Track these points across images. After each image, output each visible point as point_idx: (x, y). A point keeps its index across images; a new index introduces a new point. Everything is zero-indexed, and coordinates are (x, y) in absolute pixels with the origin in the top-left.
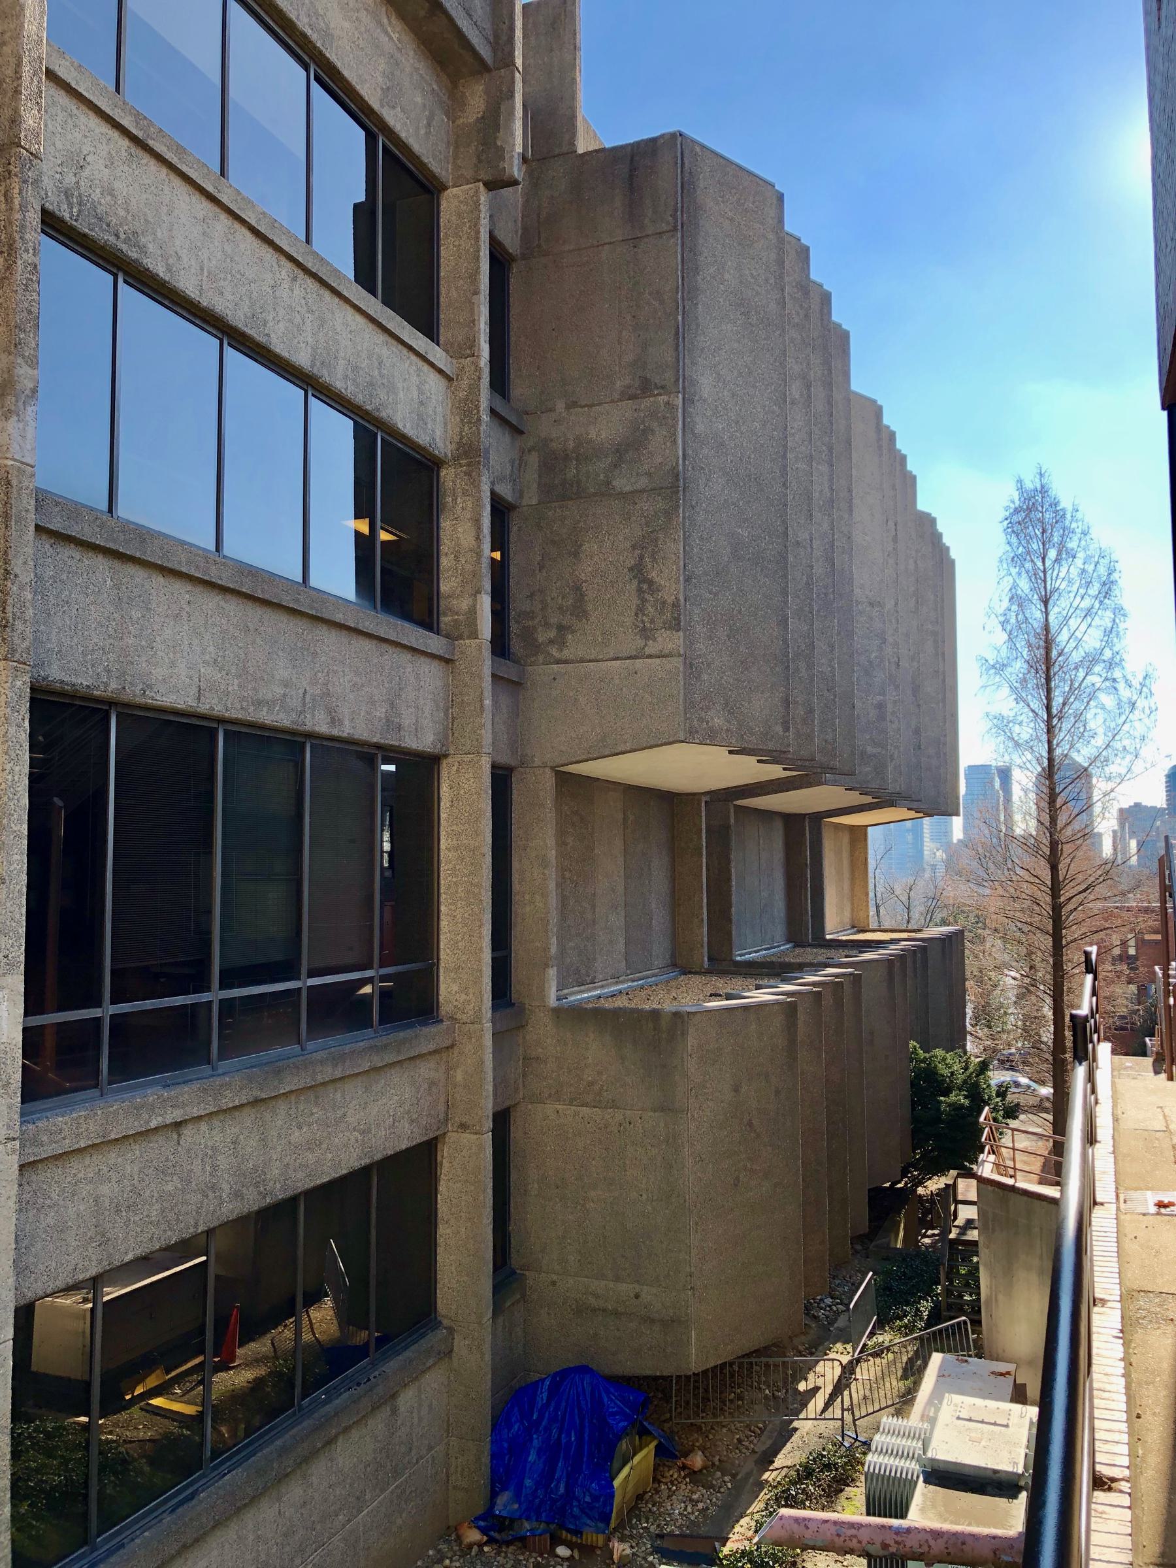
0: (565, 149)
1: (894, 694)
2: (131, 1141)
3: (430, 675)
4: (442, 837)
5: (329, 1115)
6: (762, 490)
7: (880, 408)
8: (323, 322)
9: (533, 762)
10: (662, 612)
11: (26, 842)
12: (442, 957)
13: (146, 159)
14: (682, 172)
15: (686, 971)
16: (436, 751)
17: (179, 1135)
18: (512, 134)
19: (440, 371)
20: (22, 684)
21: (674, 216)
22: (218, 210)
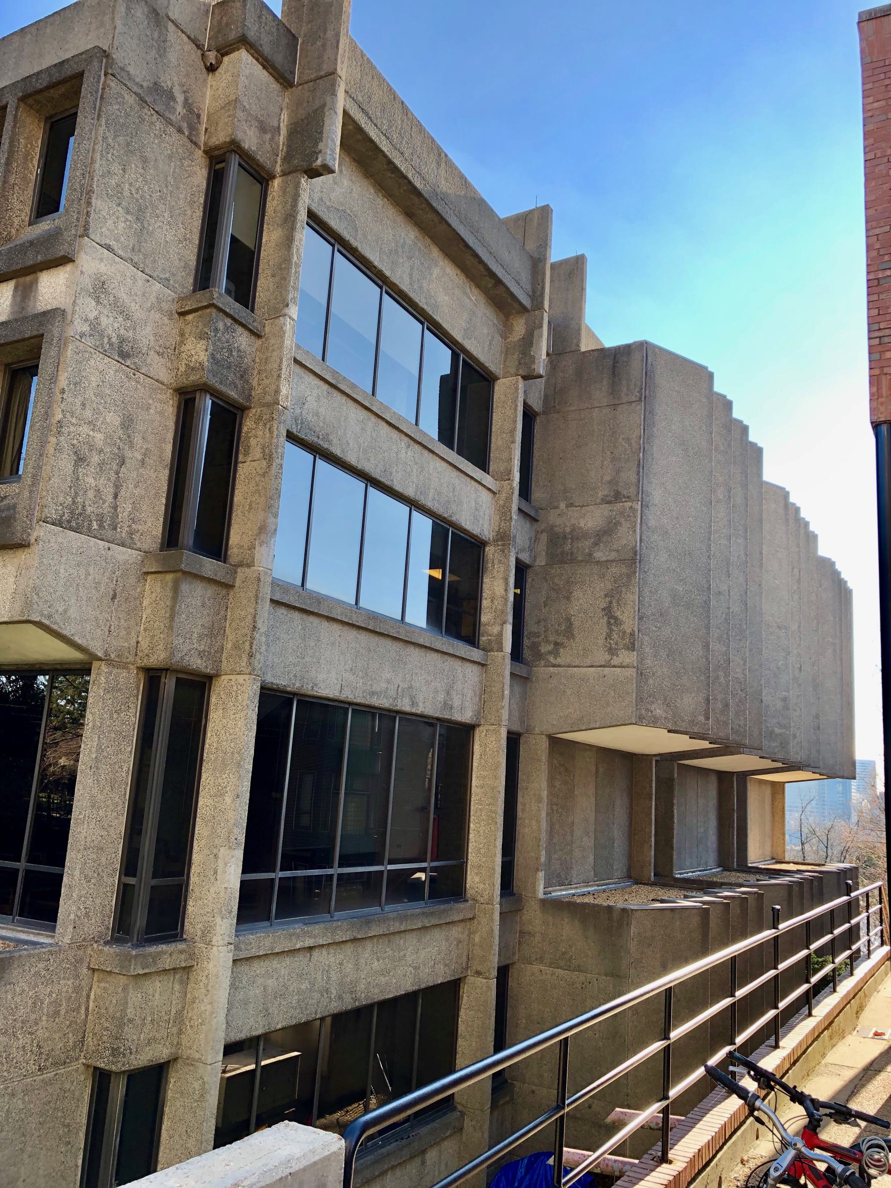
0: (574, 348)
1: (798, 690)
2: (285, 955)
3: (471, 673)
5: (395, 954)
7: (788, 493)
9: (535, 730)
11: (250, 775)
12: (469, 858)
13: (336, 393)
15: (638, 882)
16: (473, 723)
17: (311, 955)
19: (489, 489)
20: (257, 687)
22: (370, 414)
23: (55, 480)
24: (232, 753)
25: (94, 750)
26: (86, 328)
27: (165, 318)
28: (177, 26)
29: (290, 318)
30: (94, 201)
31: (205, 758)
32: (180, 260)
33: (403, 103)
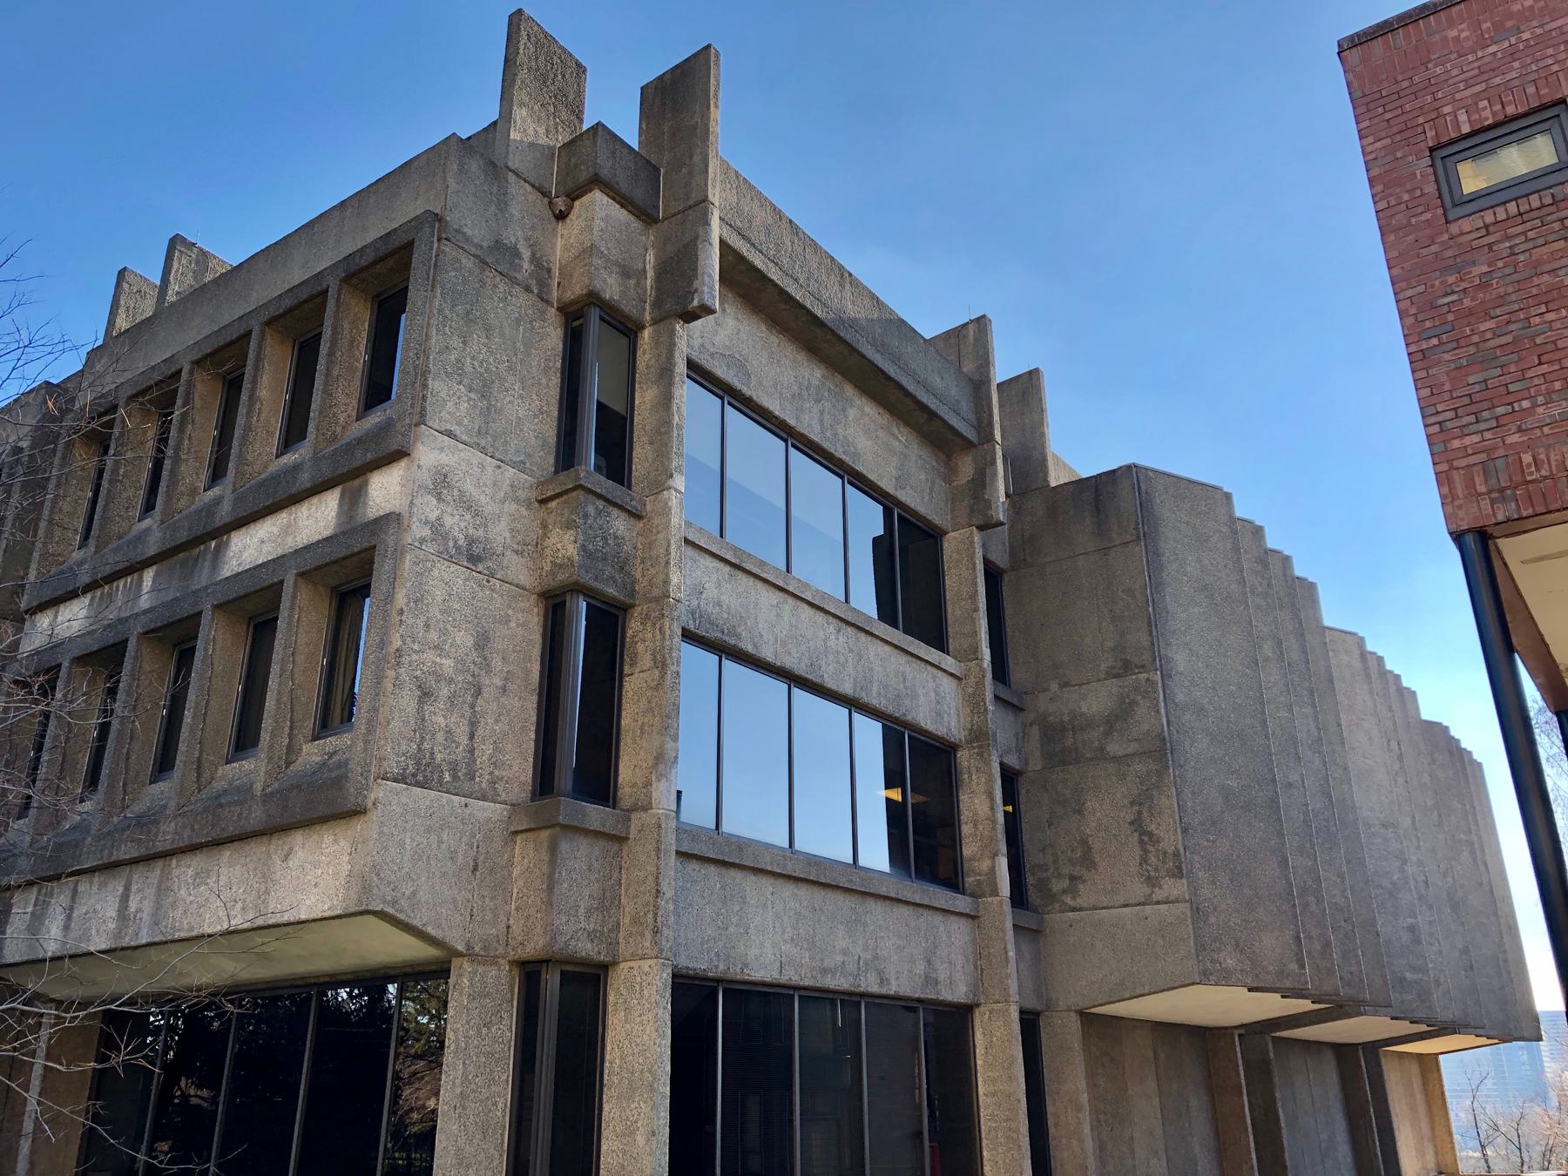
1: (1428, 914)
3: (958, 932)
4: (980, 1083)
6: (1245, 744)
8: (860, 656)
10: (1164, 863)
13: (740, 575)
14: (1139, 494)
18: (996, 490)
19: (952, 675)
20: (667, 975)
21: (1136, 529)
22: (786, 596)
23: (395, 725)
24: (642, 1072)
25: (458, 1082)
26: (426, 532)
27: (523, 509)
28: (517, 175)
29: (676, 490)
30: (430, 382)
31: (605, 1082)
32: (537, 437)
33: (791, 221)
